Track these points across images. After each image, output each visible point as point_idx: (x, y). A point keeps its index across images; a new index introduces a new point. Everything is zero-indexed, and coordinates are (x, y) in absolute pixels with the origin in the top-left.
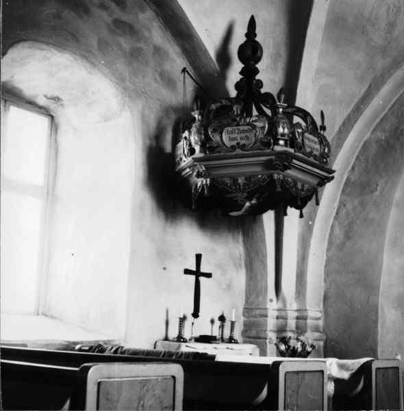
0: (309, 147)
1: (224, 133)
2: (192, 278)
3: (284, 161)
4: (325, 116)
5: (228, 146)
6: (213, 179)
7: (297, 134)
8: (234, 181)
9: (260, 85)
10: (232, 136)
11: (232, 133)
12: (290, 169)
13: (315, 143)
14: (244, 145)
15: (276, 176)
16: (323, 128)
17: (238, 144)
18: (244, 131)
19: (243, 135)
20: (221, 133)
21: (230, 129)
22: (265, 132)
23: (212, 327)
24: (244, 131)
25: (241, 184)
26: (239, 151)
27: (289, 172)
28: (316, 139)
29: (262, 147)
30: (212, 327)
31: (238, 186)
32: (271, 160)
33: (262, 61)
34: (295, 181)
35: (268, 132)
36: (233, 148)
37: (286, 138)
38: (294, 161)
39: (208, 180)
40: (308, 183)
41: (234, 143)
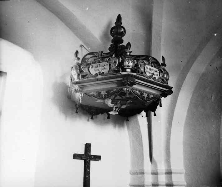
0: (150, 73)
1: (90, 67)
2: (81, 163)
3: (129, 81)
4: (165, 59)
5: (94, 74)
6: (86, 94)
7: (139, 65)
8: (99, 94)
9: (123, 46)
10: (96, 69)
11: (95, 67)
12: (135, 85)
13: (156, 71)
14: (103, 73)
15: (125, 89)
16: (164, 64)
17: (100, 72)
18: (103, 65)
19: (103, 68)
20: (89, 68)
21: (94, 65)
22: (116, 65)
23: (175, 185)
24: (103, 65)
25: (145, 97)
26: (100, 77)
27: (134, 86)
28: (157, 70)
29: (114, 73)
30: (175, 185)
31: (101, 96)
32: (121, 80)
33: (125, 36)
34: (142, 92)
35: (116, 67)
36: (96, 75)
37: (131, 67)
38: (136, 80)
39: (83, 94)
40: (152, 94)
41: (97, 72)
